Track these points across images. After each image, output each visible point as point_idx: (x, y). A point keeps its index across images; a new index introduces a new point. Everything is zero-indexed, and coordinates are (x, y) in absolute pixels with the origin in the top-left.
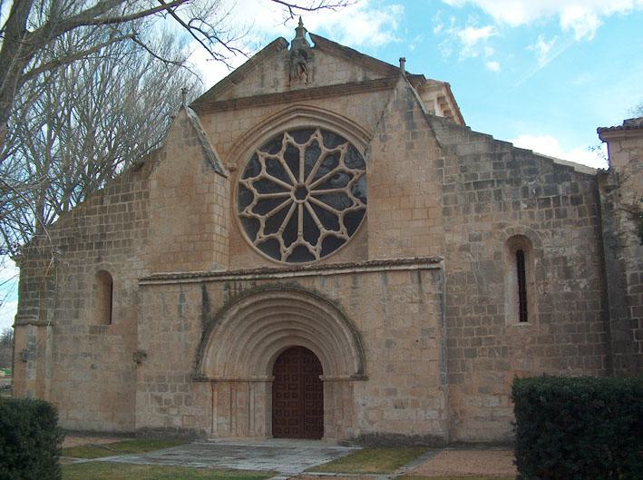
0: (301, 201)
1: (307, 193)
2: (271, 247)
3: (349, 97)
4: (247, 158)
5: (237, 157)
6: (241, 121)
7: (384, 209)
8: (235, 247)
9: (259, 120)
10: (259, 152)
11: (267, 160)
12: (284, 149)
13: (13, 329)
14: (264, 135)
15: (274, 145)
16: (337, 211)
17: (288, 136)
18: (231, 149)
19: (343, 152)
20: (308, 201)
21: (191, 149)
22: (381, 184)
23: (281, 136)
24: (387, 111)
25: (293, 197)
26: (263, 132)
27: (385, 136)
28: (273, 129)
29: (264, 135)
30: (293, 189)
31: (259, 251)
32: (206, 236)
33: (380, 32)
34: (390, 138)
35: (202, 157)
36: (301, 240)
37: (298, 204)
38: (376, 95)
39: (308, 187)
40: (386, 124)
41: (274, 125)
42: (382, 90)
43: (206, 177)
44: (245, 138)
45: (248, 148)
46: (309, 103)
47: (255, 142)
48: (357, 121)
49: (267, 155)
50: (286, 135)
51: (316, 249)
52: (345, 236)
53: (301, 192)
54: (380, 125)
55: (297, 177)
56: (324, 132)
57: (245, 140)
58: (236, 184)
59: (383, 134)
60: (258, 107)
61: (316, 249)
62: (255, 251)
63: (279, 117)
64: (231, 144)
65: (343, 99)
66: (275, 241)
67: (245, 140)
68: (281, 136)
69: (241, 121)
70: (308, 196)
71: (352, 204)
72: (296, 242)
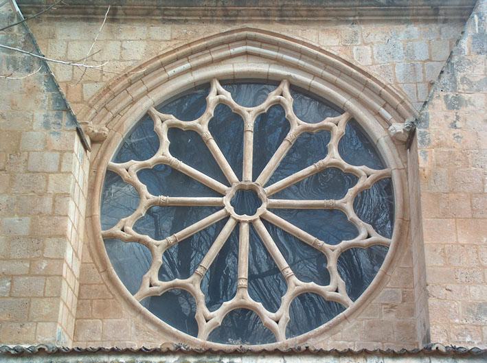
0: (246, 218)
1: (258, 202)
2: (173, 307)
3: (356, 28)
4: (130, 120)
5: (110, 115)
6: (125, 45)
7: (462, 241)
8: (89, 303)
9: (163, 48)
10: (155, 113)
11: (173, 131)
12: (211, 110)
13: (37, 350)
14: (169, 79)
15: (190, 100)
16: (326, 245)
17: (222, 89)
18: (100, 97)
19: (129, 222)
20: (238, 224)
21: (21, 77)
22: (452, 191)
23: (206, 86)
24: (460, 51)
25: (230, 208)
26: (170, 73)
27: (457, 98)
28: (192, 69)
29: (169, 79)
30: (230, 192)
31: (149, 313)
32: (44, 264)
33: (148, 111)
34: (469, 102)
35: (45, 96)
36: (244, 297)
37: (238, 223)
38: (414, 29)
39: (263, 192)
40: (459, 76)
41: (195, 62)
42: (426, 21)
43: (54, 138)
44: (132, 80)
45: (133, 102)
46: (275, 28)
47: (148, 91)
48: (374, 71)
49: (173, 119)
50: (216, 86)
51: (277, 319)
52: (343, 295)
53: (247, 200)
54: (445, 76)
55: (239, 171)
56: (296, 89)
57: (130, 84)
58: (103, 170)
59: (451, 95)
60: (164, 21)
61: (277, 319)
62: (140, 312)
63: (207, 48)
64: (100, 86)
65: (346, 30)
66: (186, 294)
67: (130, 84)
68: (206, 86)
69: (125, 45)
70: (262, 209)
71: (356, 234)
72: (234, 301)
